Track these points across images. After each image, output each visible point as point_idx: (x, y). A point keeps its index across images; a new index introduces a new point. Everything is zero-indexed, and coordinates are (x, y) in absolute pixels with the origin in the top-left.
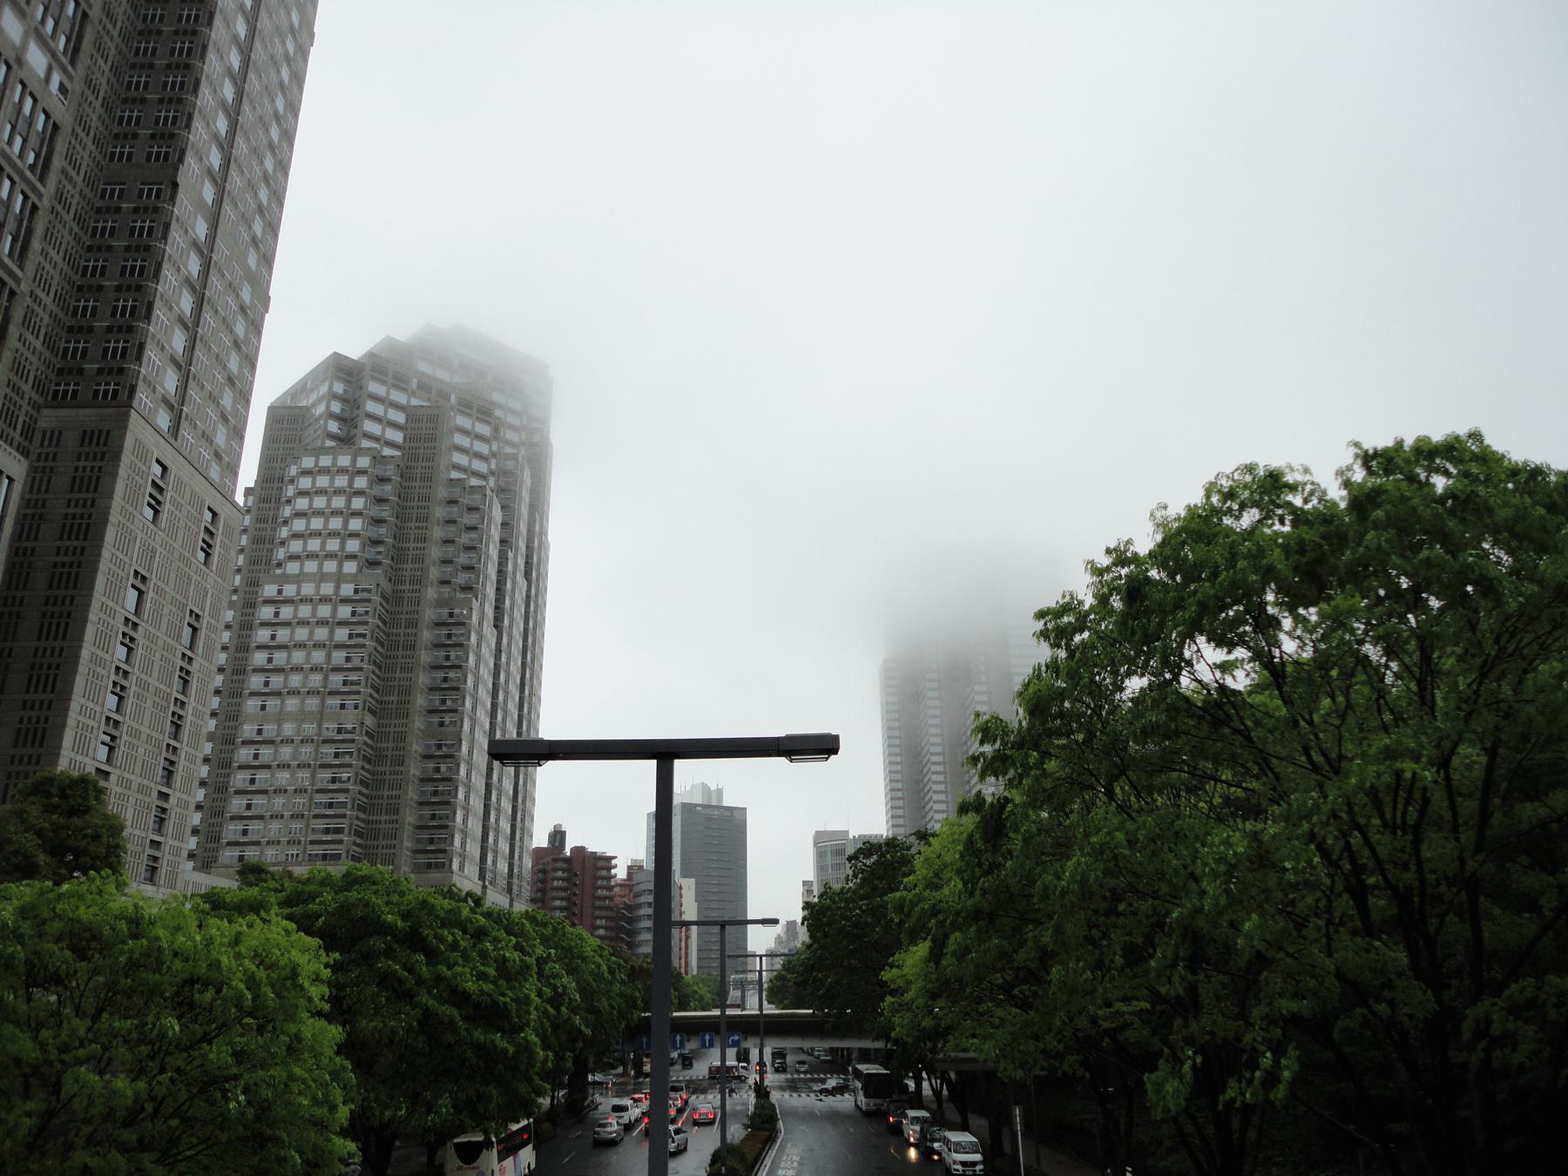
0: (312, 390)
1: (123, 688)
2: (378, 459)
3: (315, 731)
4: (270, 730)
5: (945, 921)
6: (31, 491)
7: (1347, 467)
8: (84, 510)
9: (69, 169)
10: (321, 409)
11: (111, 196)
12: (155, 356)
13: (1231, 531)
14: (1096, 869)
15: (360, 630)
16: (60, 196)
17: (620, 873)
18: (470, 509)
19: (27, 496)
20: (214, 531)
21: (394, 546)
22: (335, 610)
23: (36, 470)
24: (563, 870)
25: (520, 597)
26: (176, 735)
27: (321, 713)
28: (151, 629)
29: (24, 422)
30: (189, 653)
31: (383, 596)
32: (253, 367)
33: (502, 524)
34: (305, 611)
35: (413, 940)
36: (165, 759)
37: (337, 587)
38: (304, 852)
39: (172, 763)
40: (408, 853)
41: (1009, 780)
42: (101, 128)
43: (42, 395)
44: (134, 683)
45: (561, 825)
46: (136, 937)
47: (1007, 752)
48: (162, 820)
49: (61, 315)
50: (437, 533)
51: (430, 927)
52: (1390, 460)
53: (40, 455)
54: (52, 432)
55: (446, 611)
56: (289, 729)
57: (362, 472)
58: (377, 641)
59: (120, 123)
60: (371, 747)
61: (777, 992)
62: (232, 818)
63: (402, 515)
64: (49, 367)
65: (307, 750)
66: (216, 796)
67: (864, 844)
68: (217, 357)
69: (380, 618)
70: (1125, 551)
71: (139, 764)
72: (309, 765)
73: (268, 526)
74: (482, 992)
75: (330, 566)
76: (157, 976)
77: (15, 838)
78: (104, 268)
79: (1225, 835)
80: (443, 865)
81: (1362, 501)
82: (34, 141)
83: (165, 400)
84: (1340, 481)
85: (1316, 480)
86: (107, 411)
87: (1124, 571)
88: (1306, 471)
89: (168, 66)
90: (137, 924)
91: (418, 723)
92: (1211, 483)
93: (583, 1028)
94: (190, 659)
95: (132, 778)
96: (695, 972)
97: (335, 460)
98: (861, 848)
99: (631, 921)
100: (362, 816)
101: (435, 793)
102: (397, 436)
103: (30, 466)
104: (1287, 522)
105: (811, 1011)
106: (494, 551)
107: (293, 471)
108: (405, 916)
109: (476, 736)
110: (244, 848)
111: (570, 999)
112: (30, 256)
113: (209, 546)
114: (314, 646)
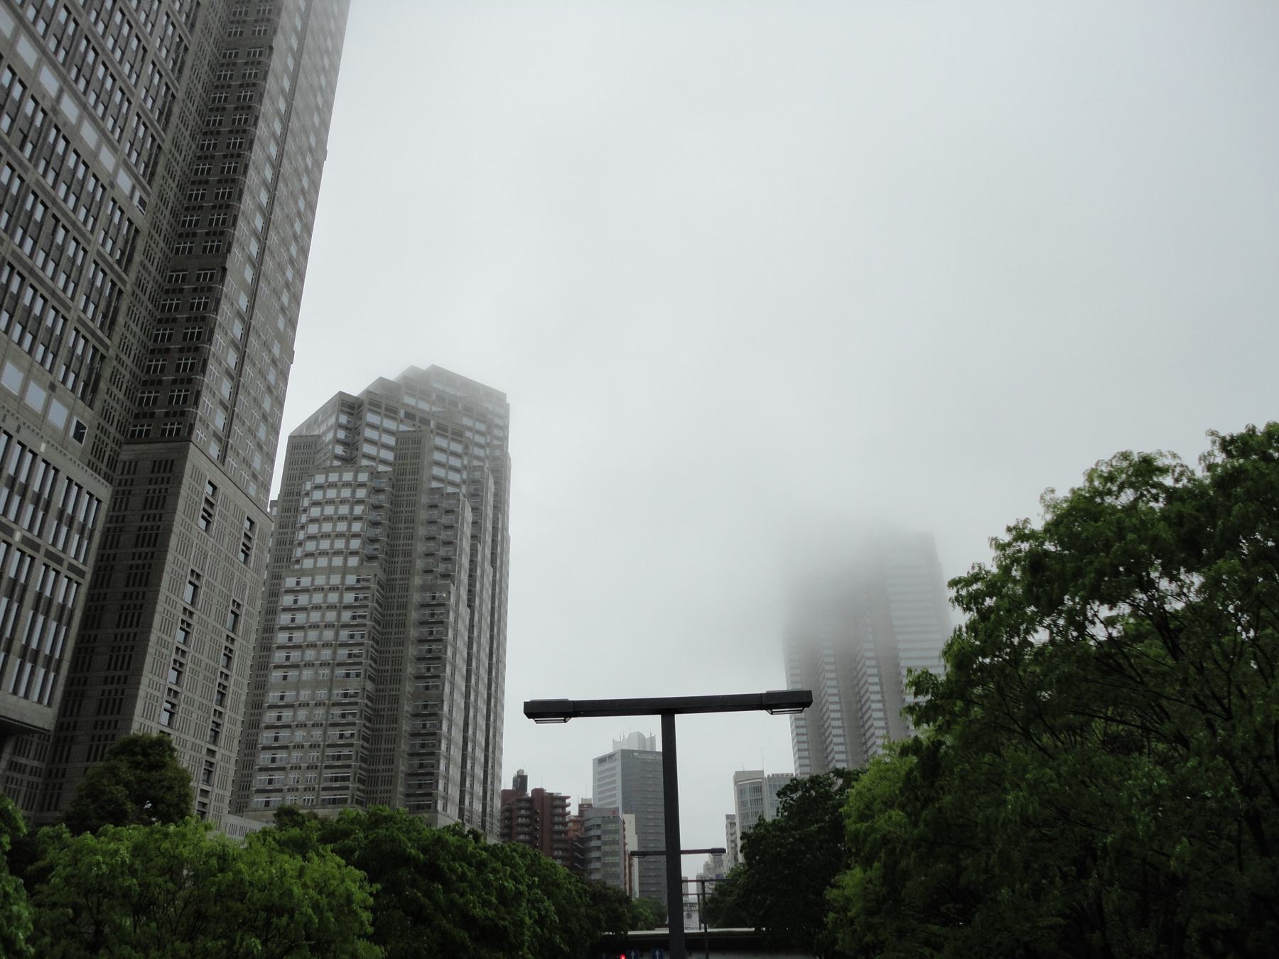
0: (323, 422)
1: (181, 665)
2: (375, 475)
3: (326, 697)
4: (290, 695)
5: (894, 849)
6: (114, 510)
7: (1208, 452)
8: (154, 523)
9: (146, 262)
10: (330, 436)
11: (177, 280)
12: (209, 400)
13: (1113, 507)
14: (1032, 802)
15: (360, 612)
16: (139, 283)
17: (573, 810)
18: (448, 512)
19: (110, 514)
20: (252, 536)
21: (388, 544)
22: (341, 597)
23: (117, 492)
24: (526, 809)
25: (488, 581)
26: (221, 702)
27: (331, 680)
28: (203, 616)
29: (110, 456)
30: (232, 635)
31: (379, 584)
32: (282, 406)
33: (473, 523)
34: (318, 598)
35: (432, 872)
36: (213, 722)
37: (343, 578)
38: (318, 797)
39: (218, 725)
40: (402, 797)
41: (939, 726)
42: (169, 229)
43: (123, 435)
44: (190, 660)
45: (523, 771)
46: (222, 870)
47: (938, 702)
48: (210, 772)
49: (138, 372)
50: (422, 531)
51: (444, 860)
52: (1245, 443)
53: (121, 481)
54: (131, 463)
55: (428, 595)
56: (305, 695)
57: (362, 485)
58: (375, 621)
59: (183, 225)
60: (370, 708)
61: (709, 911)
62: (260, 770)
63: (394, 518)
64: (128, 413)
65: (320, 712)
66: (247, 751)
67: (792, 780)
68: (255, 400)
69: (377, 602)
70: (1024, 529)
71: (193, 725)
72: (321, 725)
73: (289, 530)
74: (487, 918)
75: (338, 561)
76: (239, 904)
77: (108, 789)
78: (170, 335)
79: (1146, 769)
80: (429, 806)
81: (1225, 481)
82: (120, 243)
83: (215, 435)
84: (1203, 465)
85: (1184, 463)
86: (170, 445)
87: (1025, 546)
88: (1174, 456)
89: (220, 181)
90: (224, 858)
91: (408, 688)
92: (1093, 470)
93: (562, 946)
94: (233, 640)
95: (188, 738)
96: (637, 896)
97: (341, 476)
98: (788, 786)
99: (583, 852)
100: (364, 766)
101: (423, 746)
102: (389, 456)
103: (113, 491)
104: (1161, 500)
105: (753, 929)
106: (466, 545)
107: (308, 486)
108: (424, 850)
109: (455, 697)
110: (270, 794)
111: (551, 920)
112: (117, 329)
113: (248, 548)
114: (325, 626)
